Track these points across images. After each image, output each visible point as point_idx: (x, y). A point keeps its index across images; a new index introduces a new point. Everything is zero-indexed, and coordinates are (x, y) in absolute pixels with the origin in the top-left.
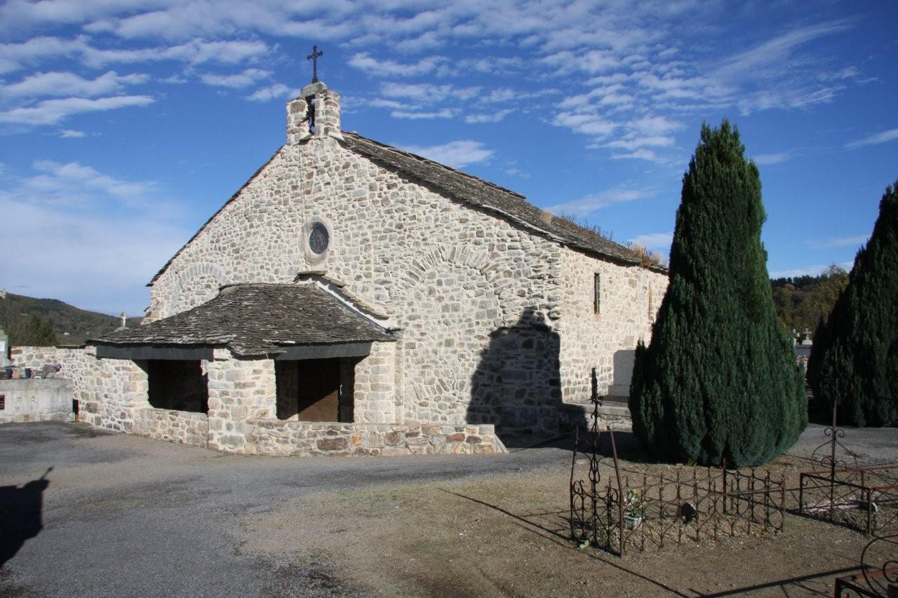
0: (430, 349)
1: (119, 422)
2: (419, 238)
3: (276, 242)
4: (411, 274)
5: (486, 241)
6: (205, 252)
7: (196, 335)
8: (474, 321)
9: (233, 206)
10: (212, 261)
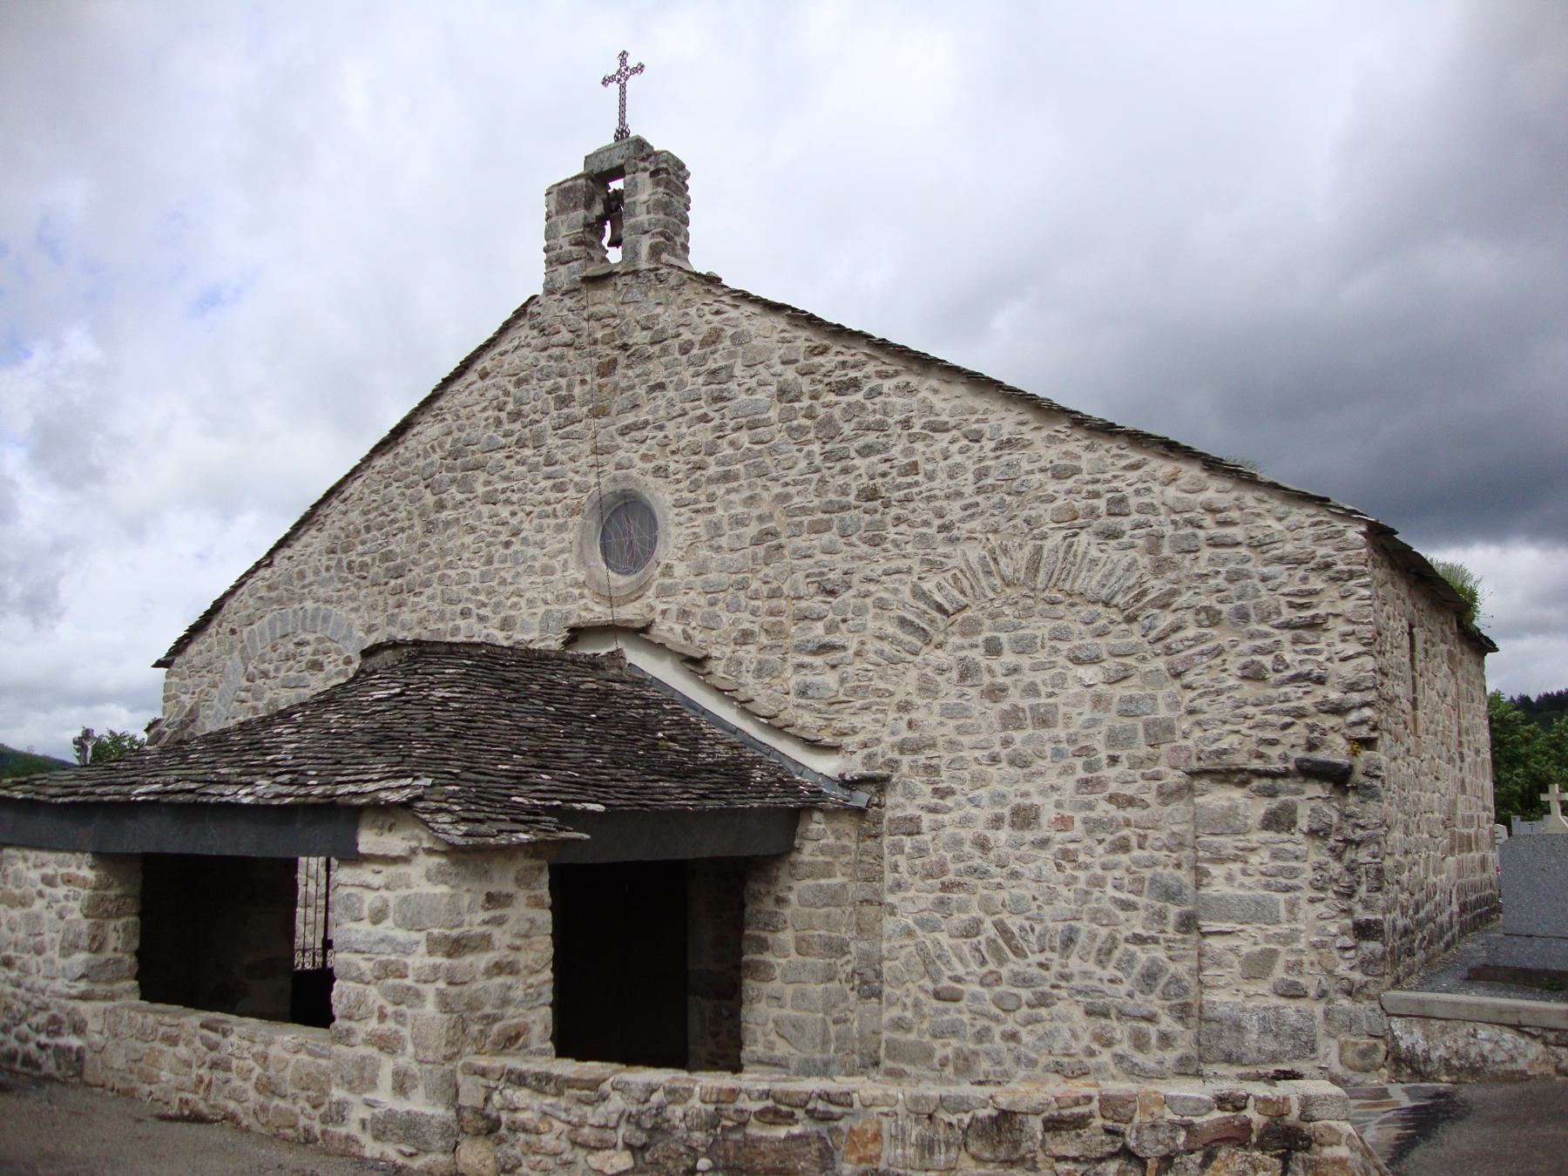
0: (966, 834)
1: (42, 1047)
2: (926, 523)
3: (507, 545)
4: (903, 622)
5: (1138, 526)
6: (310, 578)
7: (298, 777)
8: (1103, 754)
9: (390, 456)
10: (327, 601)
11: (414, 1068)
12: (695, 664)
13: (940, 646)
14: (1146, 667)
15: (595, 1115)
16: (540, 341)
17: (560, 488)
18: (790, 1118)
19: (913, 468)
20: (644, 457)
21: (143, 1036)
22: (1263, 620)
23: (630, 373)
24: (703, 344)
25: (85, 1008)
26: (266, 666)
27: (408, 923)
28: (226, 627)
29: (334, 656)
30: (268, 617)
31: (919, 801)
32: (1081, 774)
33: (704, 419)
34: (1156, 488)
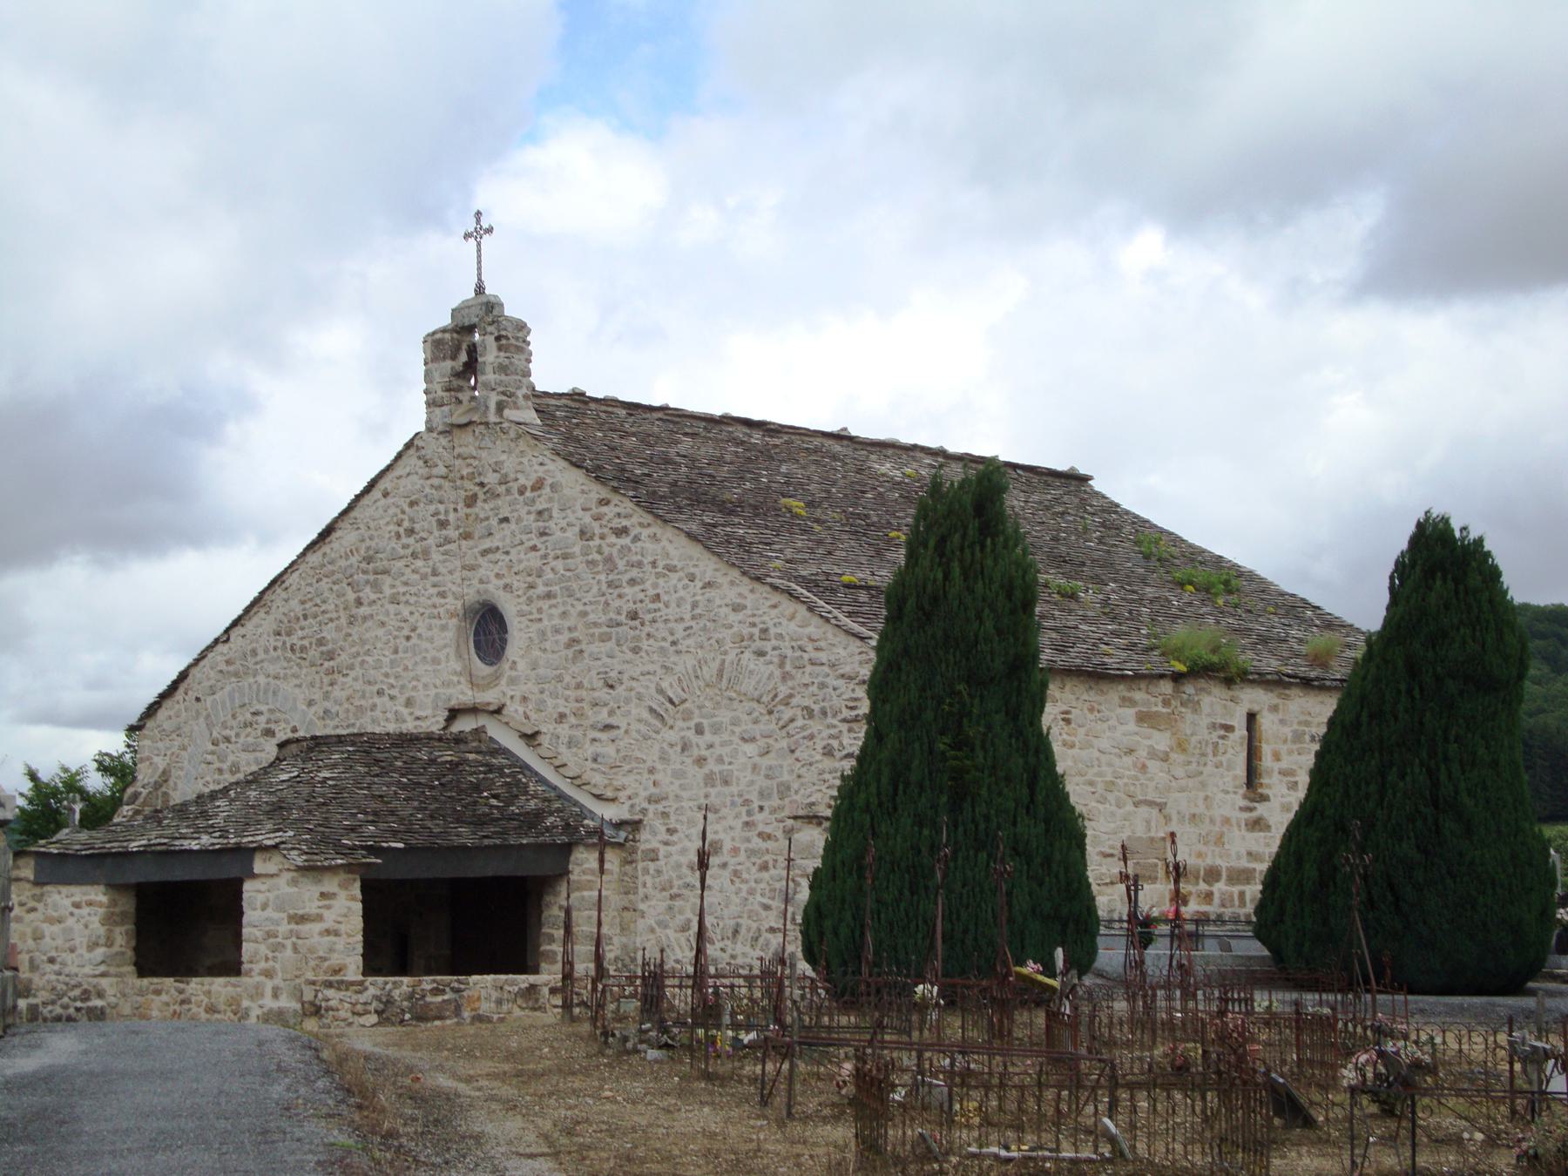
1: (78, 1010)
2: (664, 639)
3: (408, 638)
4: (652, 710)
5: (774, 649)
6: (261, 656)
7: (224, 833)
8: (756, 805)
10: (276, 678)
11: (282, 984)
12: (531, 738)
13: (671, 727)
14: (777, 746)
15: (362, 998)
16: (424, 471)
17: (442, 595)
18: (443, 992)
19: (657, 597)
20: (498, 576)
21: (141, 993)
22: (834, 716)
23: (486, 506)
24: (534, 489)
25: (104, 983)
26: (227, 732)
27: (300, 921)
28: (192, 695)
29: (283, 725)
30: (228, 688)
31: (659, 837)
32: (745, 818)
33: (534, 548)
34: (785, 622)
